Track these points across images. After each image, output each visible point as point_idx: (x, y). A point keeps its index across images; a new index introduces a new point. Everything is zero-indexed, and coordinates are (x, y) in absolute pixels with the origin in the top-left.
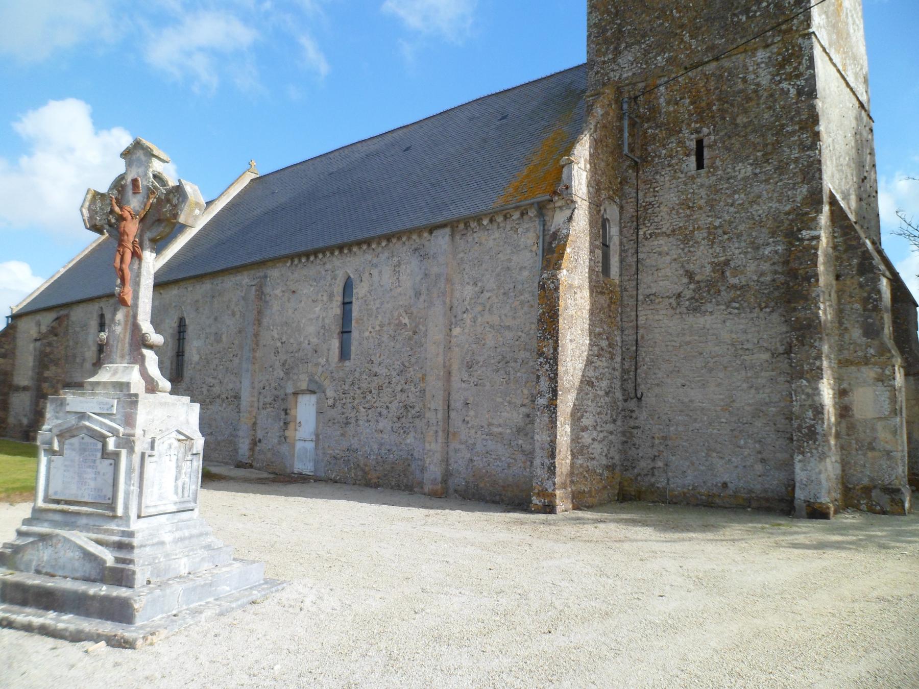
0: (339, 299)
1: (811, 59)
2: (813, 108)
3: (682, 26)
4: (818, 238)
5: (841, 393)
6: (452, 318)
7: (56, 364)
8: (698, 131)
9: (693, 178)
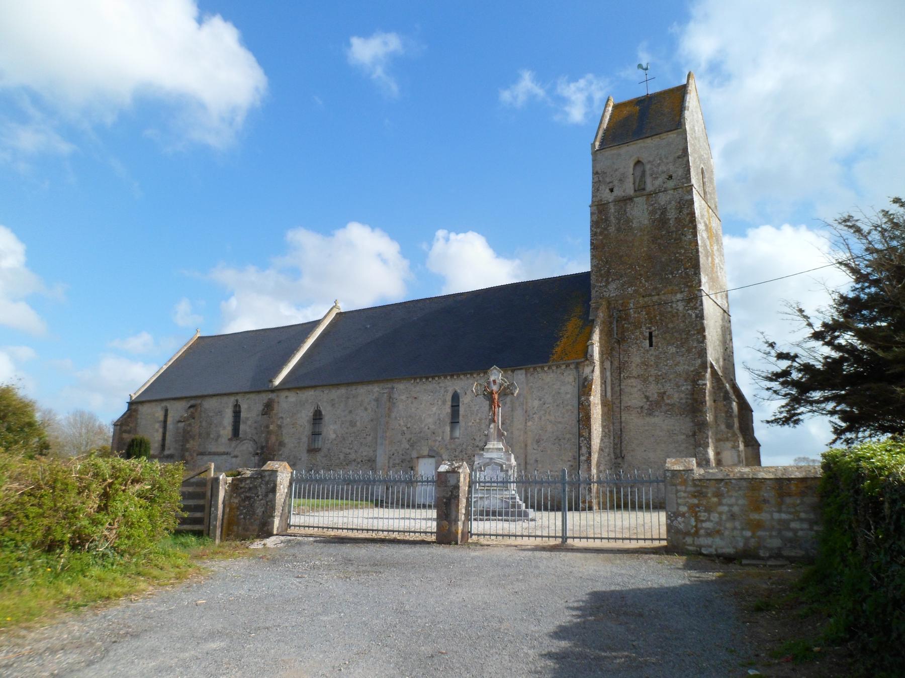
0: (449, 403)
1: (701, 301)
2: (702, 324)
3: (641, 275)
4: (705, 384)
5: (717, 454)
6: (528, 417)
7: (194, 439)
8: (650, 328)
9: (648, 351)
